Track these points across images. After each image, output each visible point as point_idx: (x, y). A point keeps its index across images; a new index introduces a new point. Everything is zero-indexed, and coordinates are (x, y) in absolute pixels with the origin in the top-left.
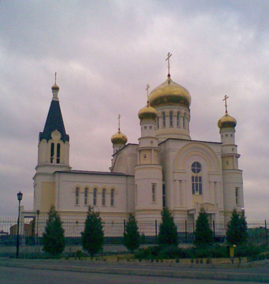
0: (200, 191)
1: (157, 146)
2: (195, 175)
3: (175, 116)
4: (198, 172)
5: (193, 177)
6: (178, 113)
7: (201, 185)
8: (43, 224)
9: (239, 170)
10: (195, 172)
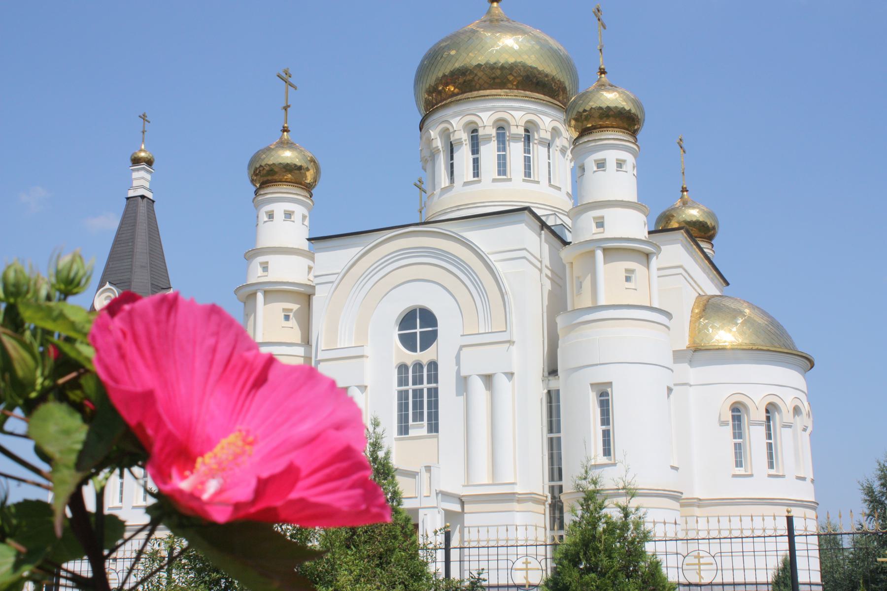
0: (429, 419)
1: (646, 234)
2: (410, 357)
3: (515, 138)
4: (424, 347)
5: (402, 368)
6: (526, 130)
7: (434, 393)
8: (771, 544)
9: (577, 309)
10: (414, 349)
